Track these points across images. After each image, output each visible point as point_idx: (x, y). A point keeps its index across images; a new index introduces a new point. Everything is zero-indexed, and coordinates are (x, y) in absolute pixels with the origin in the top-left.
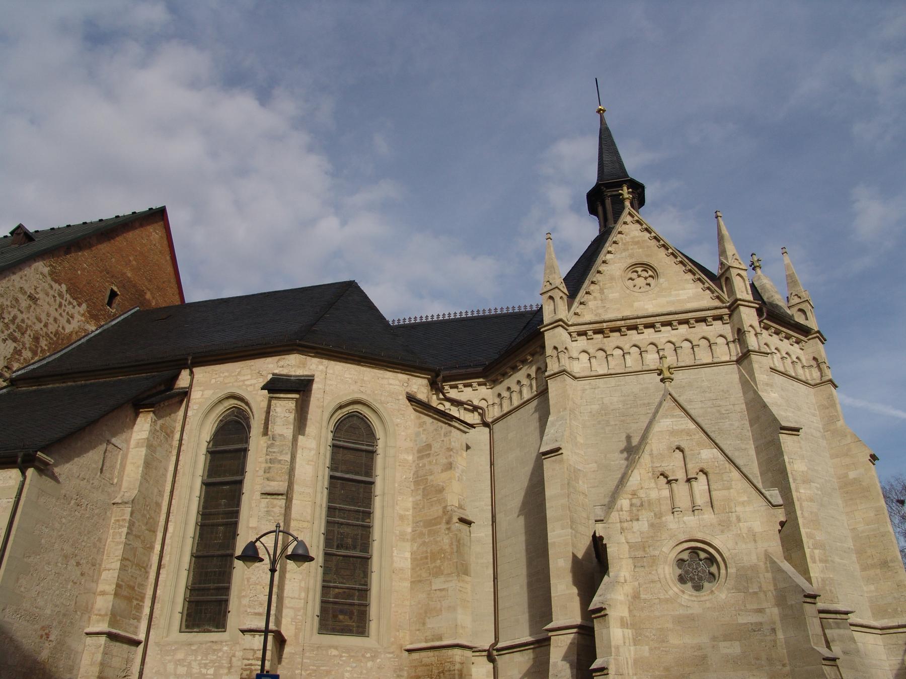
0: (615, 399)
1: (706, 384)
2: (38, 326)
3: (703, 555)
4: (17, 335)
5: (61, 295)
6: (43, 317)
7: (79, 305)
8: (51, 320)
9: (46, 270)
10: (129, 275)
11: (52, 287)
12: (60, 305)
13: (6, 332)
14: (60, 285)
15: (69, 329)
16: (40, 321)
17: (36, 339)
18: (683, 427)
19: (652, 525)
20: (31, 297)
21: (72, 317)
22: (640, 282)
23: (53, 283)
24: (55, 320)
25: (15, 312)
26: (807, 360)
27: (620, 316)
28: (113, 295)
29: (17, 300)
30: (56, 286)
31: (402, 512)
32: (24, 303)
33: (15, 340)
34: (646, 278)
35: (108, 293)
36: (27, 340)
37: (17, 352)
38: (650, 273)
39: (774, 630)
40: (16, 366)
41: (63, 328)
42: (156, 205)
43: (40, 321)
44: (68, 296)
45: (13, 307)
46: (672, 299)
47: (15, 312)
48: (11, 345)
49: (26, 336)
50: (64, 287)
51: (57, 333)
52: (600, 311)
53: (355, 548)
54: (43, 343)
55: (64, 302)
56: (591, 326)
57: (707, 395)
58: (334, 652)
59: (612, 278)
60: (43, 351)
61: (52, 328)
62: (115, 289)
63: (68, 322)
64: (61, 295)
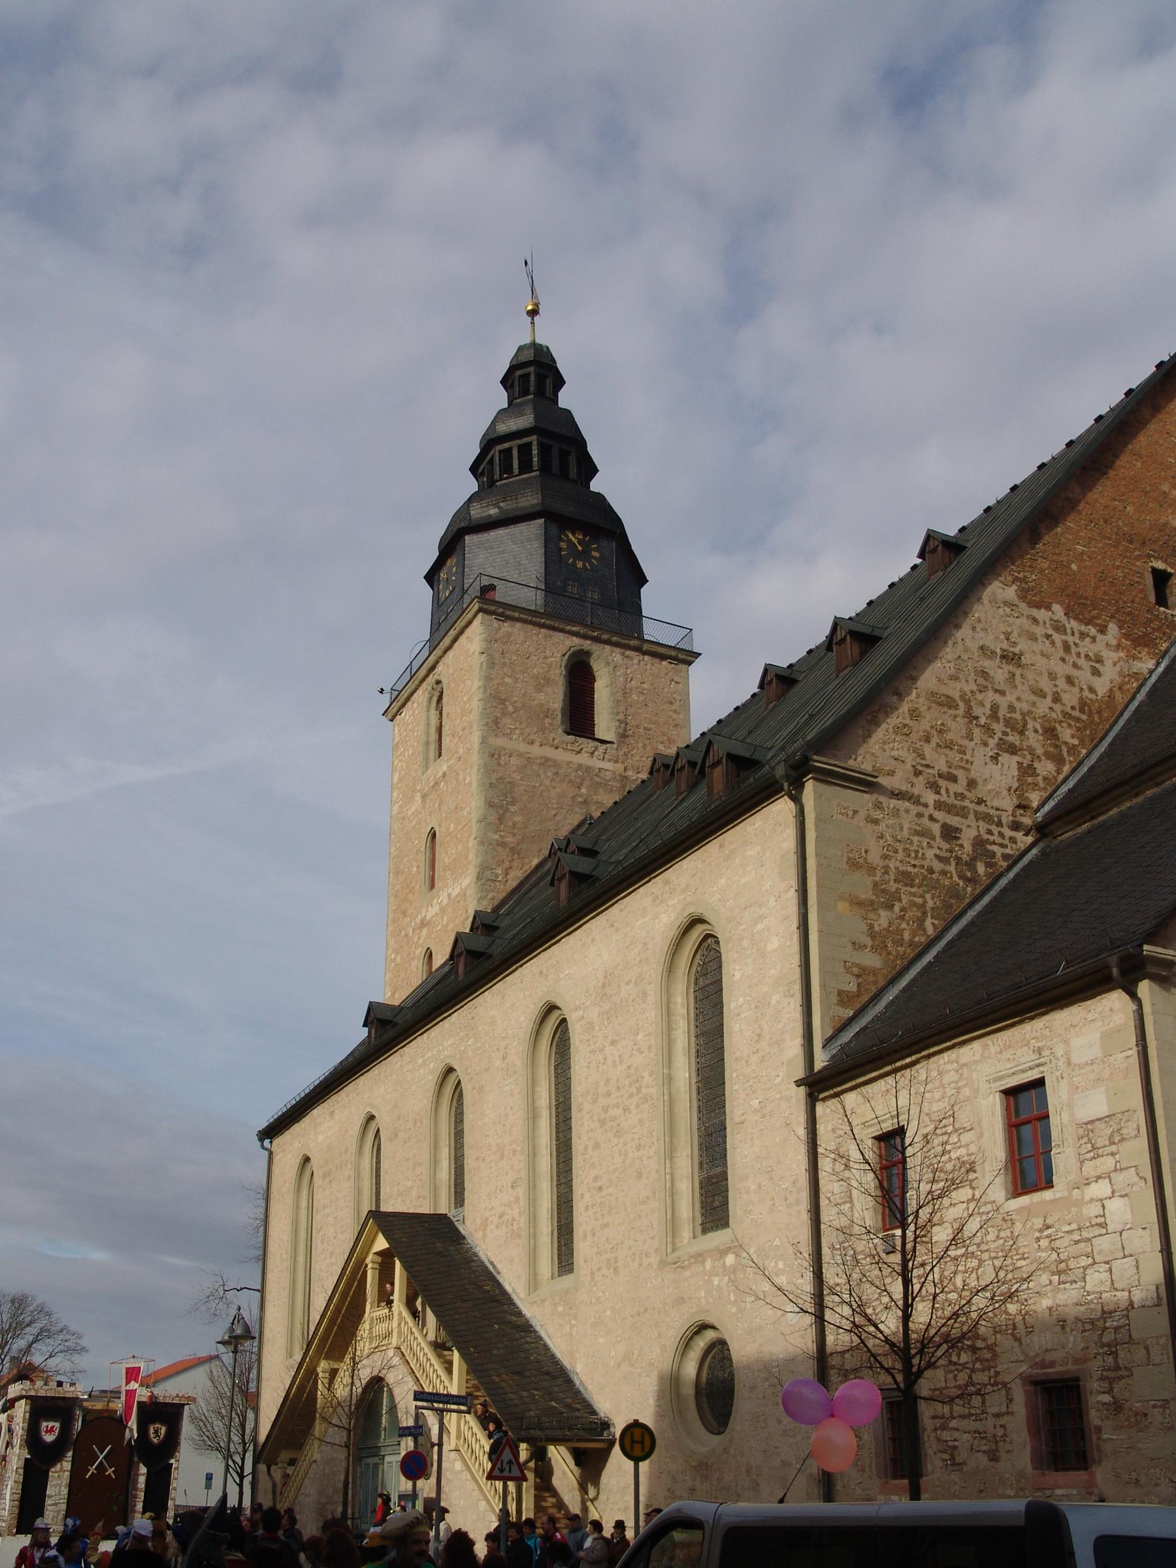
2: (1043, 707)
4: (1013, 738)
6: (1045, 684)
7: (1103, 630)
8: (1062, 684)
9: (1011, 593)
13: (992, 742)
15: (1102, 687)
16: (1043, 695)
17: (1050, 732)
20: (1007, 657)
21: (1099, 660)
23: (1035, 612)
24: (1070, 680)
29: (984, 674)
30: (1042, 614)
32: (999, 673)
33: (1013, 750)
35: (1149, 580)
36: (1034, 740)
37: (1026, 771)
40: (1035, 798)
41: (1092, 690)
44: (1074, 623)
48: (1010, 762)
49: (1030, 733)
54: (1066, 734)
55: (1070, 639)
60: (1072, 749)
61: (1070, 698)
62: (1160, 565)
63: (1096, 673)
64: (1059, 628)
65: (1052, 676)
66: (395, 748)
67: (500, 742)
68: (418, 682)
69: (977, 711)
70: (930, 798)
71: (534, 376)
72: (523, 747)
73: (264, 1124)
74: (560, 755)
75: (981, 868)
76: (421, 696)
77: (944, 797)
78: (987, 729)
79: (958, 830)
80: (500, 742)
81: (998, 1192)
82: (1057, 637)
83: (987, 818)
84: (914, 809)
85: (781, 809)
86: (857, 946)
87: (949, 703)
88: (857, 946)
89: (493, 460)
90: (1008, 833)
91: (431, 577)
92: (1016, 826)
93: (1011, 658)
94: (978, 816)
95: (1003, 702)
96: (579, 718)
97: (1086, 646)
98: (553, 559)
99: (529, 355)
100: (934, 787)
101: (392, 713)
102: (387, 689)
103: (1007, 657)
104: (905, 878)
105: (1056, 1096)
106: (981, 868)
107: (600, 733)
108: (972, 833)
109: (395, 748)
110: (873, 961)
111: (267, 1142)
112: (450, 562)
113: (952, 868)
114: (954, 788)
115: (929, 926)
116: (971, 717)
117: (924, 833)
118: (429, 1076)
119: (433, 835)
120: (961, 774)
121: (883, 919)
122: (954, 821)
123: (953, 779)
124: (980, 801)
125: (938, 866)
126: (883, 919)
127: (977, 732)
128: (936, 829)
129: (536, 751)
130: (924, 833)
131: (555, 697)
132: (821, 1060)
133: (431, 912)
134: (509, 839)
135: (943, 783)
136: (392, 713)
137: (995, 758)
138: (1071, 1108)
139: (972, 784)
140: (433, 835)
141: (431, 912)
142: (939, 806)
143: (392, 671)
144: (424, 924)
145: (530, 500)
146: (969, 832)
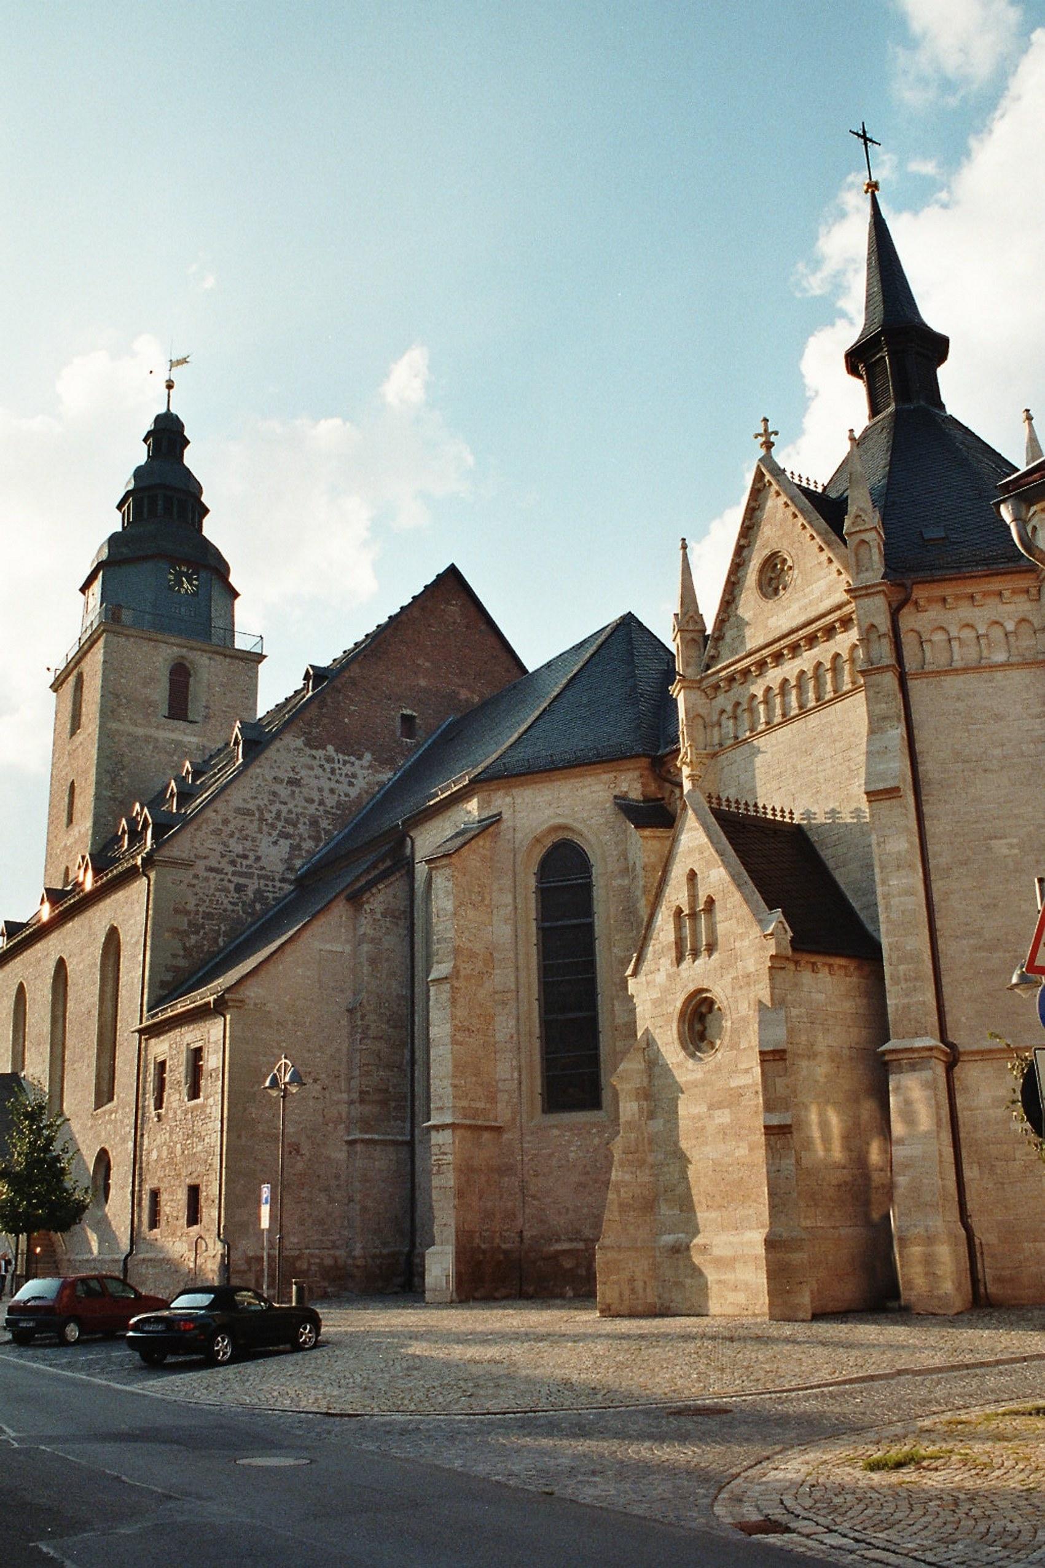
2: (312, 809)
4: (290, 830)
5: (329, 760)
6: (316, 796)
7: (360, 758)
8: (326, 794)
9: (299, 743)
10: (423, 683)
12: (333, 771)
13: (275, 833)
14: (324, 748)
15: (353, 792)
16: (311, 801)
17: (314, 823)
20: (292, 782)
21: (354, 776)
23: (314, 752)
24: (332, 791)
28: (407, 720)
29: (275, 794)
30: (320, 753)
32: (284, 791)
33: (287, 836)
36: (303, 829)
40: (298, 863)
41: (347, 795)
43: (311, 801)
44: (341, 756)
45: (272, 802)
48: (285, 844)
50: (330, 748)
54: (324, 824)
55: (336, 766)
60: (327, 832)
61: (331, 801)
62: (408, 712)
64: (329, 760)
65: (320, 790)
69: (267, 815)
70: (230, 869)
71: (167, 436)
75: (258, 906)
76: (72, 679)
77: (239, 869)
78: (273, 826)
82: (327, 766)
83: (266, 877)
87: (248, 813)
88: (174, 956)
90: (278, 884)
92: (283, 880)
97: (348, 769)
100: (233, 863)
103: (292, 782)
104: (208, 916)
106: (258, 906)
110: (182, 963)
116: (262, 820)
117: (226, 890)
122: (242, 881)
123: (246, 857)
124: (262, 868)
128: (232, 887)
130: (226, 890)
131: (160, 693)
135: (239, 860)
138: (212, 1061)
142: (234, 874)
146: (253, 885)
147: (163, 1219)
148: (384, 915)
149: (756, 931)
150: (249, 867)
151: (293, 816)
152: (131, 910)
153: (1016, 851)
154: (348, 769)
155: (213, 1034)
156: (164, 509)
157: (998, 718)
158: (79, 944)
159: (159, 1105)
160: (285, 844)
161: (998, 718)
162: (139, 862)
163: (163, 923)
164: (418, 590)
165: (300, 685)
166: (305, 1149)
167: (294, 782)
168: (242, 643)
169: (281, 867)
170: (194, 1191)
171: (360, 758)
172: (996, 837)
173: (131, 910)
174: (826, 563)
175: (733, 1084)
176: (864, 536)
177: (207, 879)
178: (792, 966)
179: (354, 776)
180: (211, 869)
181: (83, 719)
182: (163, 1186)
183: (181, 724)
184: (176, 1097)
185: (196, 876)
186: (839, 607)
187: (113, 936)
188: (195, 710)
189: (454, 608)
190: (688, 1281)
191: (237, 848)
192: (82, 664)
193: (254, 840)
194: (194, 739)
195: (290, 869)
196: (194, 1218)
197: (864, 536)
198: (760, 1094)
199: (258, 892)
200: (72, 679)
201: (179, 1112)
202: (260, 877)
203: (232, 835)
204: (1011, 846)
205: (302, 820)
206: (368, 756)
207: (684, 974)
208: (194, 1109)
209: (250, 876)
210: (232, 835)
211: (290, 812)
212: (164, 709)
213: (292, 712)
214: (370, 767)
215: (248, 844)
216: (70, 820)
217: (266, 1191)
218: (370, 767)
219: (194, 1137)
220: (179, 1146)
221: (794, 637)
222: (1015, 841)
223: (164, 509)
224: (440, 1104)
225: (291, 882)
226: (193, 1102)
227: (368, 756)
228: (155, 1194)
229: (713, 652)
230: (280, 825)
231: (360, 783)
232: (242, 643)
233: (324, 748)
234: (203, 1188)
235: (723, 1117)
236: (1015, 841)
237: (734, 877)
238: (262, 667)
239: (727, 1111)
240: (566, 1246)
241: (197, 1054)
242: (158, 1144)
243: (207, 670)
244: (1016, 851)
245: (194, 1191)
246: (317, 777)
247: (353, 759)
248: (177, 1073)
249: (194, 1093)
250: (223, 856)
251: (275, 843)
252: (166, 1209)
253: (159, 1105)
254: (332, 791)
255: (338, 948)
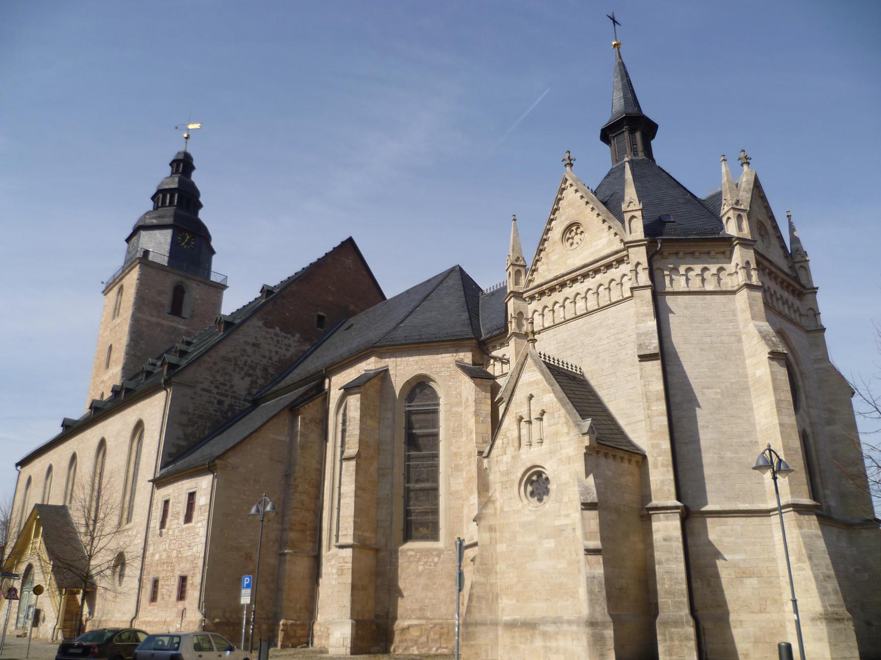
0: (553, 347)
1: (612, 321)
2: (265, 361)
3: (534, 478)
4: (251, 372)
5: (276, 335)
6: (267, 354)
7: (293, 336)
8: (273, 354)
9: (260, 323)
10: (330, 299)
11: (268, 333)
12: (278, 342)
13: (242, 373)
14: (274, 328)
15: (288, 355)
16: (264, 357)
17: (265, 369)
18: (535, 378)
19: (513, 457)
20: (254, 345)
21: (290, 346)
22: (577, 238)
23: (268, 330)
24: (277, 352)
25: (245, 358)
26: (679, 281)
27: (552, 276)
28: (321, 318)
29: (244, 350)
30: (271, 331)
31: (455, 451)
32: (250, 350)
33: (249, 375)
34: (576, 234)
35: (316, 319)
36: (259, 372)
37: (253, 383)
38: (574, 228)
39: (574, 529)
40: (254, 391)
41: (284, 356)
42: (345, 238)
43: (264, 357)
44: (283, 334)
45: (242, 355)
46: (593, 250)
47: (245, 358)
48: (248, 380)
49: (258, 370)
50: (277, 329)
51: (280, 361)
52: (546, 274)
53: (428, 480)
54: (271, 370)
55: (280, 339)
56: (536, 290)
57: (612, 331)
58: (412, 553)
59: (554, 243)
60: (272, 375)
61: (275, 358)
62: (321, 314)
63: (287, 350)
64: (276, 335)
65: (270, 351)
66: (105, 307)
67: (140, 315)
68: (114, 284)
69: (239, 363)
70: (215, 391)
71: (183, 165)
72: (149, 318)
73: (18, 460)
74: (166, 323)
75: (230, 414)
76: (116, 289)
77: (220, 391)
78: (242, 369)
79: (223, 401)
80: (140, 315)
81: (182, 522)
82: (275, 338)
83: (235, 397)
84: (209, 394)
85: (164, 393)
86: (179, 439)
87: (229, 360)
88: (179, 439)
89: (160, 196)
90: (242, 402)
91: (128, 240)
92: (245, 400)
93: (256, 345)
94: (232, 397)
95: (249, 360)
96: (176, 309)
97: (286, 341)
98: (174, 244)
99: (181, 157)
100: (217, 387)
101: (106, 292)
102: (105, 282)
103: (254, 345)
104: (201, 417)
105: (197, 496)
106: (230, 414)
107: (184, 315)
108: (229, 402)
109: (105, 307)
110: (183, 443)
111: (19, 468)
112: (135, 238)
113: (219, 414)
114: (225, 388)
115: (206, 432)
116: (236, 364)
117: (211, 403)
118: (96, 442)
119: (111, 347)
120: (228, 384)
121: (190, 430)
122: (223, 398)
123: (225, 385)
124: (234, 392)
125: (213, 413)
126: (190, 430)
127: (237, 370)
128: (215, 401)
129: (154, 320)
130: (211, 403)
131: (167, 300)
132: (158, 475)
133: (106, 378)
134: (138, 354)
135: (221, 386)
136: (106, 292)
137: (242, 378)
138: (202, 500)
139: (232, 386)
140: (111, 347)
141: (106, 378)
142: (218, 393)
143: (108, 277)
144: (103, 382)
145: (169, 220)
146: (227, 401)
147: (159, 597)
148: (311, 421)
149: (575, 432)
150: (226, 390)
151: (254, 364)
152: (153, 410)
153: (719, 396)
154: (286, 341)
155: (203, 485)
156: (179, 204)
157: (708, 321)
158: (115, 429)
159: (163, 524)
160: (248, 380)
161: (708, 321)
162: (163, 381)
163: (176, 419)
164: (330, 249)
165: (259, 295)
166: (256, 557)
167: (256, 345)
168: (214, 278)
169: (244, 393)
170: (183, 579)
171: (293, 336)
172: (707, 388)
173: (153, 410)
174: (607, 229)
175: (557, 523)
176: (634, 213)
177: (201, 396)
178: (595, 454)
179: (290, 346)
180: (204, 390)
181: (121, 310)
182: (161, 576)
183: (177, 319)
184: (176, 522)
185: (195, 393)
186: (617, 252)
187: (139, 426)
188: (186, 311)
189: (349, 262)
190: (522, 646)
191: (220, 379)
192: (124, 280)
193: (231, 376)
194: (184, 328)
195: (249, 394)
196: (181, 596)
197: (634, 213)
198: (193, 594)
199: (230, 405)
200: (116, 289)
201: (176, 531)
202: (232, 397)
203: (218, 372)
204: (716, 393)
205: (259, 367)
206: (298, 336)
207: (523, 457)
208: (187, 529)
209: (226, 396)
210: (218, 372)
211: (252, 362)
212: (168, 309)
213: (250, 312)
214: (299, 341)
215: (227, 377)
216: (108, 366)
217: (247, 580)
218: (299, 341)
219: (187, 545)
220: (175, 552)
221: (566, 278)
222: (719, 390)
223: (179, 204)
224: (345, 533)
225: (250, 402)
226: (187, 525)
227: (298, 336)
228: (156, 582)
229: (530, 278)
230: (246, 368)
231: (293, 350)
232: (214, 278)
233: (274, 328)
234: (189, 578)
235: (550, 544)
236: (719, 390)
237: (560, 400)
238: (226, 293)
239: (552, 541)
240: (415, 622)
241: (192, 496)
242: (156, 553)
243: (194, 292)
244: (719, 396)
245: (183, 579)
246: (269, 344)
247: (289, 336)
248: (179, 507)
249: (188, 518)
250: (212, 383)
251: (242, 378)
252: (161, 590)
253: (163, 524)
254: (277, 352)
255: (282, 438)
